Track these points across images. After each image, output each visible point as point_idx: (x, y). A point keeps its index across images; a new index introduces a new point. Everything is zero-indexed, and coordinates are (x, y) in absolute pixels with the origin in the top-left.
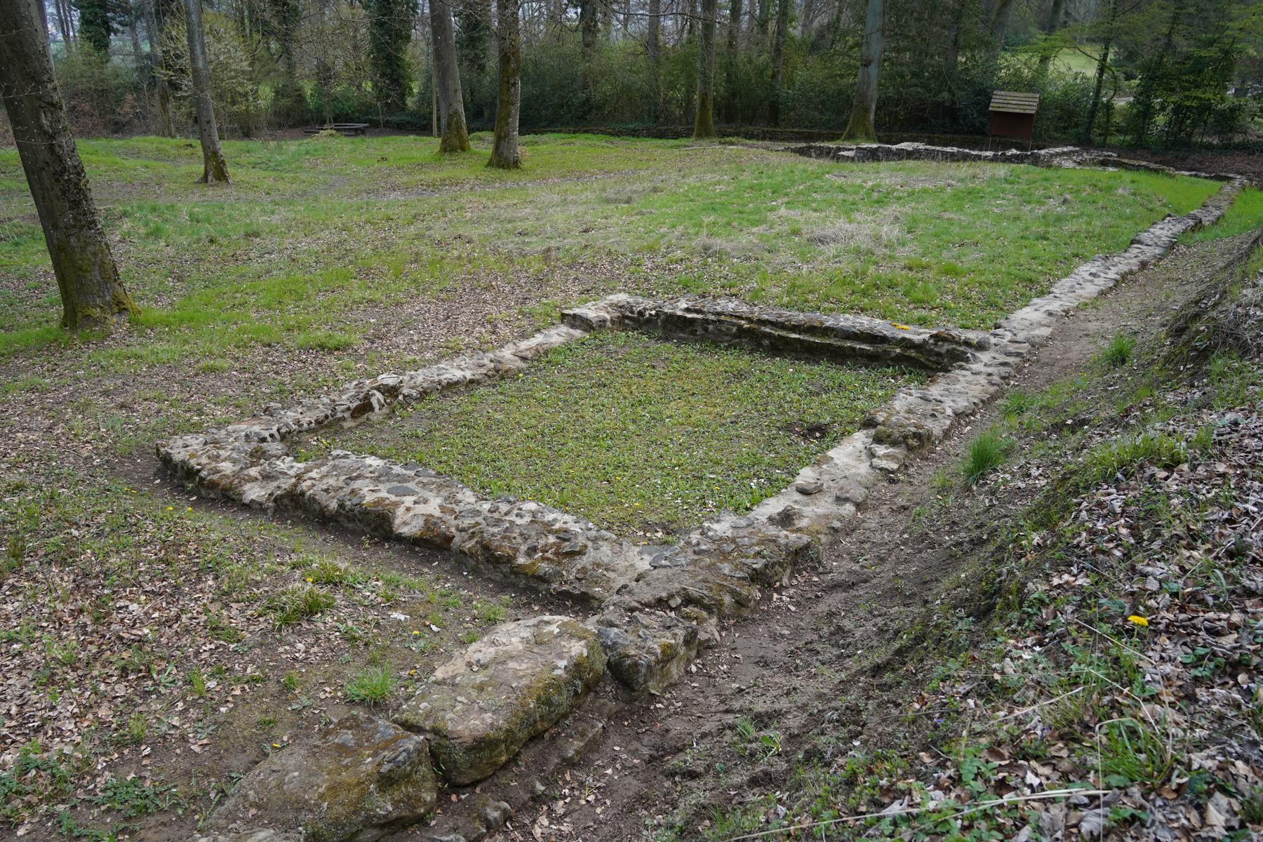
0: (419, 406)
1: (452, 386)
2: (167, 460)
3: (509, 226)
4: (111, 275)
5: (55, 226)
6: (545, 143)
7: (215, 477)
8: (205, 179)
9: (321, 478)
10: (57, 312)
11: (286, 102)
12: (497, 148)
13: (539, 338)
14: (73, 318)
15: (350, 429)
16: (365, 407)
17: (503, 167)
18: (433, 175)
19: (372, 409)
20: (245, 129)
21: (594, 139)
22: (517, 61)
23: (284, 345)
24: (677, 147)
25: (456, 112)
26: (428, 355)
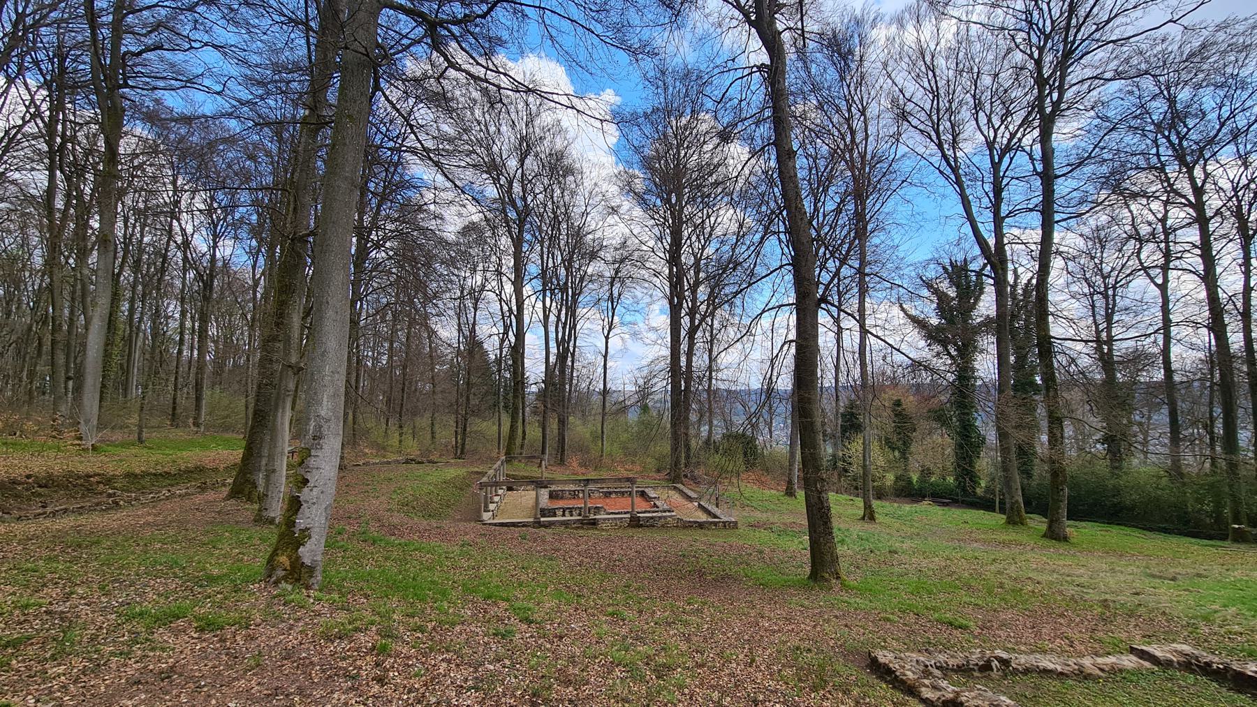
0: (1025, 678)
1: (1046, 672)
2: (874, 661)
3: (1069, 579)
4: (835, 560)
5: (815, 532)
6: (1085, 528)
7: (904, 678)
8: (863, 518)
9: (973, 698)
10: (808, 570)
11: (903, 483)
12: (1050, 527)
13: (1111, 660)
14: (815, 575)
15: (978, 677)
16: (986, 667)
17: (1055, 539)
18: (1004, 537)
19: (992, 670)
20: (880, 495)
21: (1128, 530)
22: (1065, 477)
23: (927, 617)
24: (1212, 546)
25: (1017, 501)
26: (1023, 648)
